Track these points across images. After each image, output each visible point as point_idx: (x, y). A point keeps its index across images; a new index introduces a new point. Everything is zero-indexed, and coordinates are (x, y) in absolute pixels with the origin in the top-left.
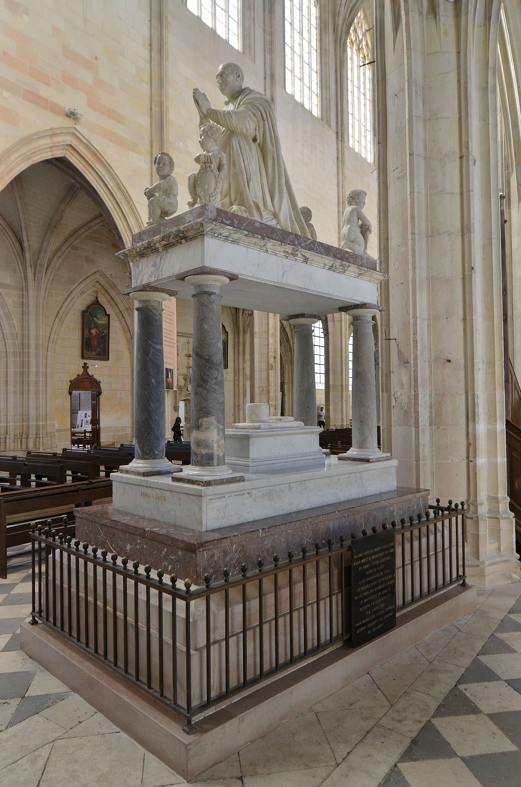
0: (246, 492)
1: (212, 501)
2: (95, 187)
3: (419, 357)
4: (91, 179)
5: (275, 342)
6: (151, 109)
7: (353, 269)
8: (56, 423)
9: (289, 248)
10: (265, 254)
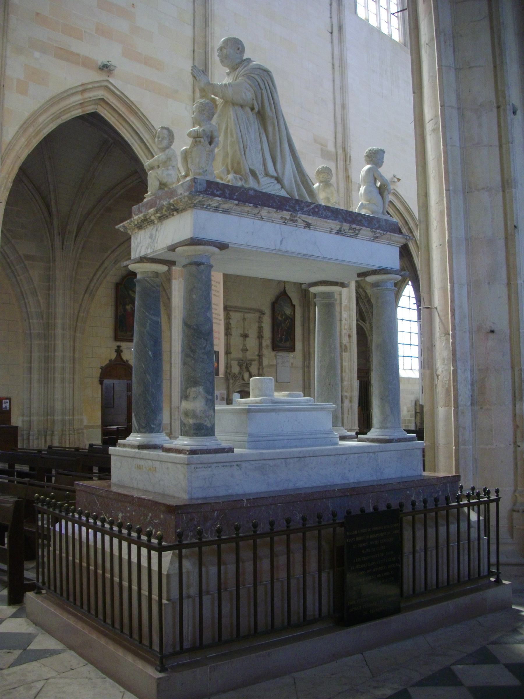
0: (235, 464)
1: (197, 470)
2: (129, 142)
3: (457, 328)
4: (124, 134)
5: (350, 316)
6: (194, 51)
7: (366, 232)
8: (85, 418)
9: (287, 215)
10: (260, 223)
